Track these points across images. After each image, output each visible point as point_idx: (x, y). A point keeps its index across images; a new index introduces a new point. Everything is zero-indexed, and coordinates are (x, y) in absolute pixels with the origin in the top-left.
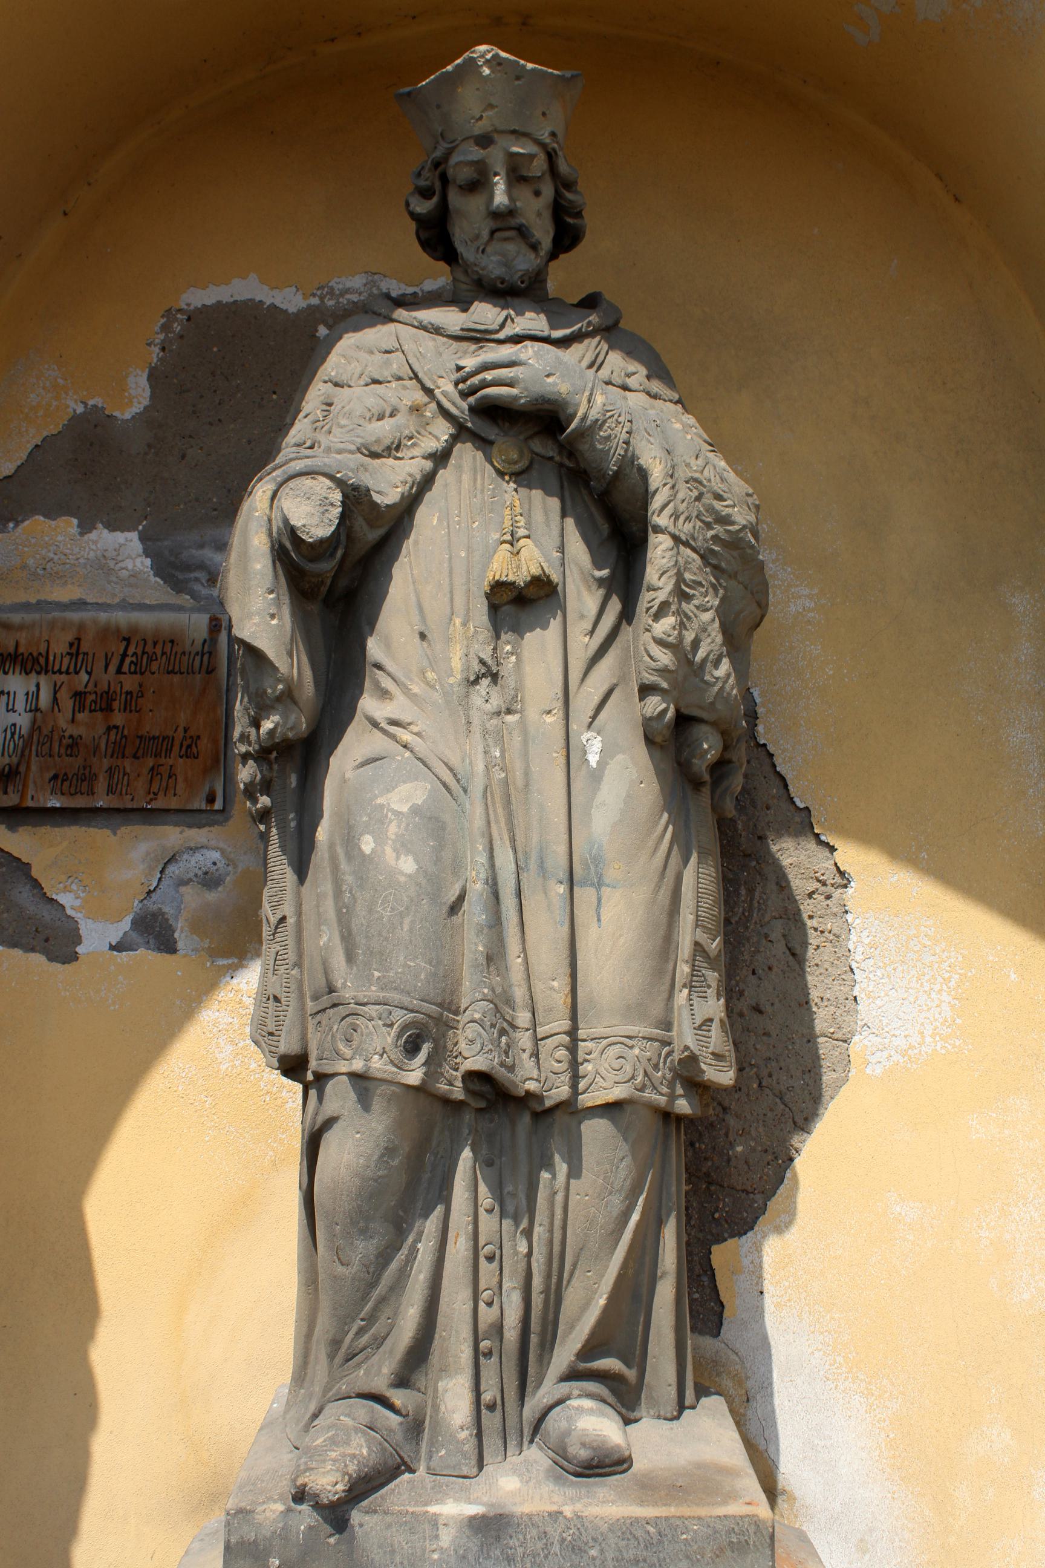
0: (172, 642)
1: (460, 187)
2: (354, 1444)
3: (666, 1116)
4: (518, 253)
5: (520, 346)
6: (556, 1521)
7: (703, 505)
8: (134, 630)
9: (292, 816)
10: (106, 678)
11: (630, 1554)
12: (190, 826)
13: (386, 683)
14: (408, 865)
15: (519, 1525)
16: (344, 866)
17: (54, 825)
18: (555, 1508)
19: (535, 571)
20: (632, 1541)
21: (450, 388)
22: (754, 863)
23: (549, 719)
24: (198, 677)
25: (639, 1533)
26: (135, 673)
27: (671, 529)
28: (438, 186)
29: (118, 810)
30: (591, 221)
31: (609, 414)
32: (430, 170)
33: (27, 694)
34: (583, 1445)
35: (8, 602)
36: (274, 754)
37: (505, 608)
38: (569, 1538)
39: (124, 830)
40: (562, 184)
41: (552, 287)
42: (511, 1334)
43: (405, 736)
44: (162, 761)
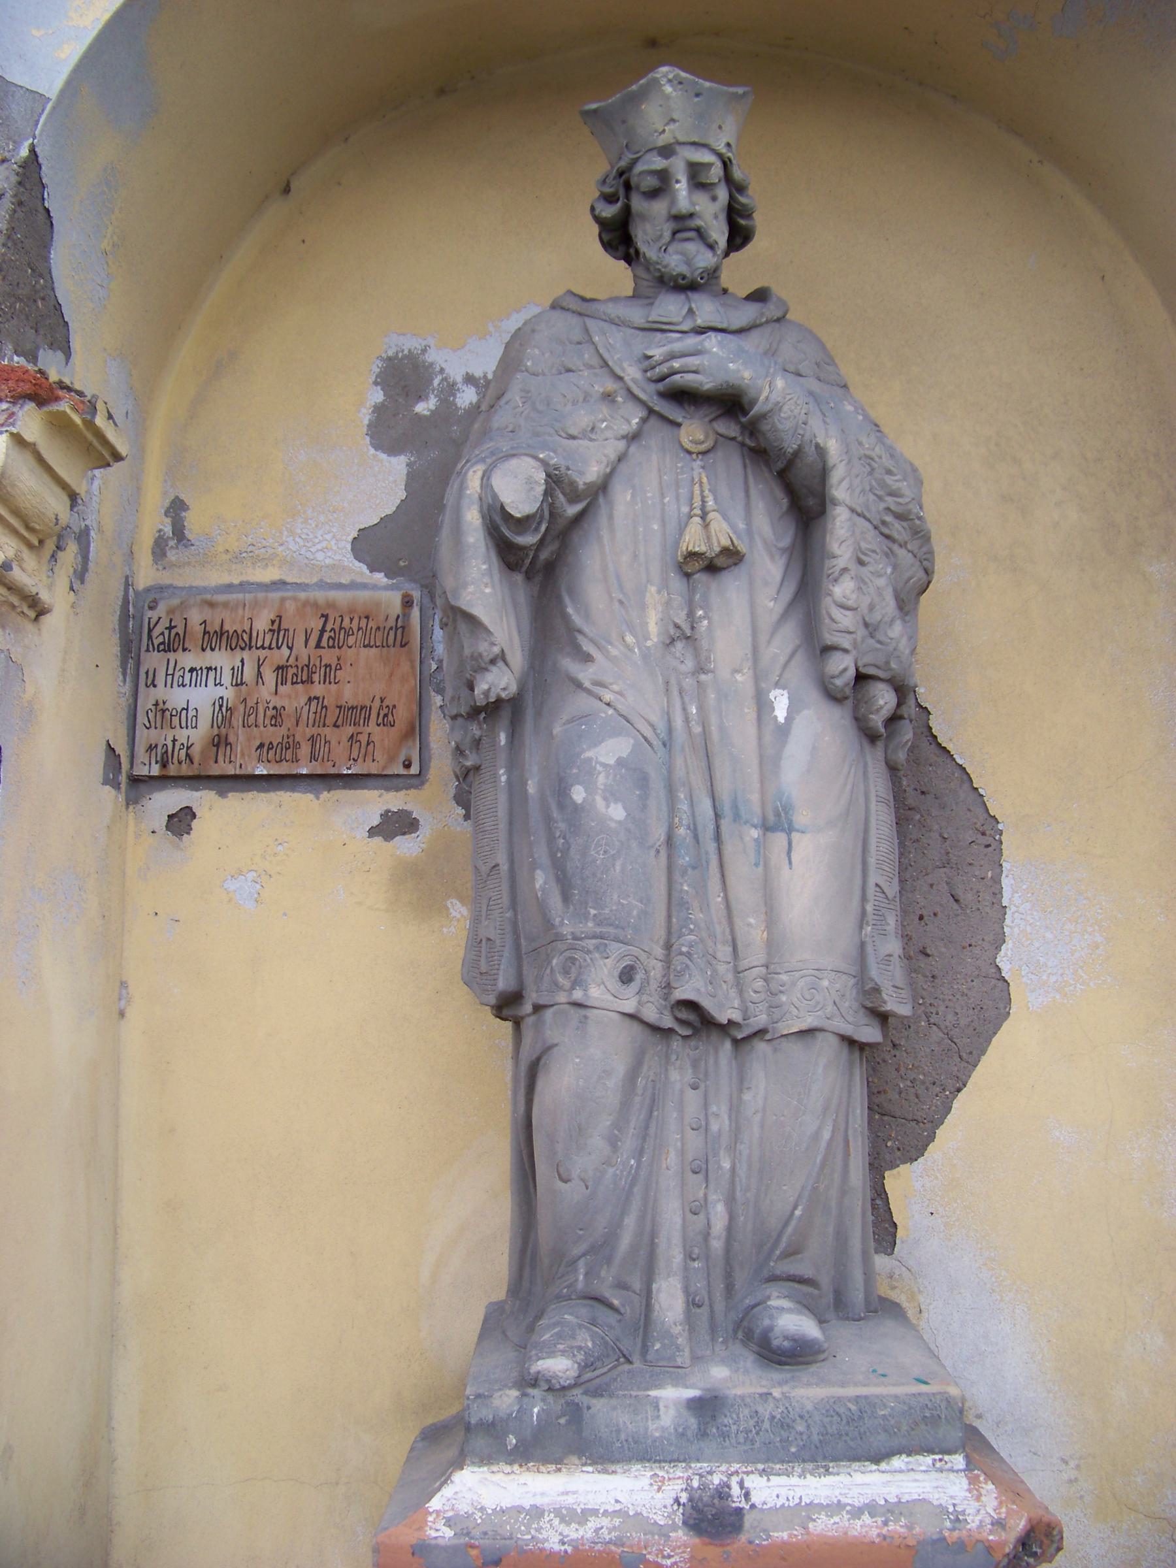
0: (367, 617)
1: (644, 193)
2: (579, 1338)
3: (850, 1042)
4: (698, 252)
5: (703, 336)
6: (766, 1401)
7: (876, 480)
8: (332, 605)
9: (502, 771)
10: (303, 652)
11: (833, 1429)
12: (388, 789)
13: (587, 647)
14: (617, 812)
15: (733, 1406)
16: (555, 814)
17: (259, 791)
18: (765, 1390)
19: (725, 542)
20: (836, 1418)
21: (638, 375)
22: (918, 817)
23: (739, 677)
24: (392, 650)
25: (842, 1410)
26: (333, 647)
27: (848, 502)
28: (622, 192)
30: (759, 220)
31: (788, 397)
32: (614, 178)
33: (233, 669)
34: (786, 1338)
35: (213, 584)
36: (483, 715)
37: (697, 576)
38: (778, 1416)
39: (325, 795)
40: (735, 187)
41: (725, 279)
42: (717, 1245)
43: (608, 697)
44: (361, 729)
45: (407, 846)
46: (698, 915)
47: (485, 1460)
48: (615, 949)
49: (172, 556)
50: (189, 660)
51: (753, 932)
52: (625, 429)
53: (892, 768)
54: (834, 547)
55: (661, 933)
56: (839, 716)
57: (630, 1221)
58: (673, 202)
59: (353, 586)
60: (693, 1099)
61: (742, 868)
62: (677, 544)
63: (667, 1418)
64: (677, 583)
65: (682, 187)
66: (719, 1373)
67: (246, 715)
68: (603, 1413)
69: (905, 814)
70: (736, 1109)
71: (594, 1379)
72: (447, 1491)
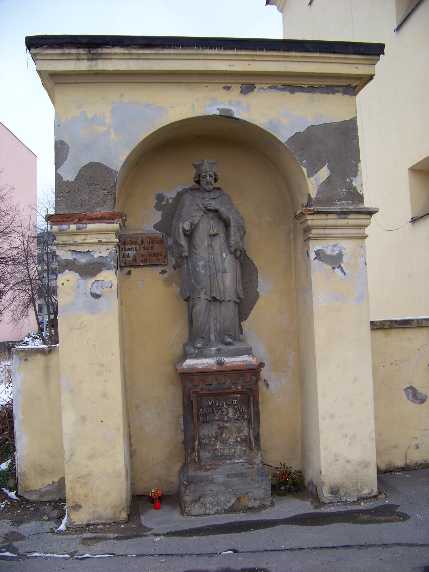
3: (235, 302)
8: (151, 237)
14: (203, 272)
29: (145, 265)
39: (152, 268)
42: (218, 330)
43: (201, 255)
45: (166, 275)
46: (214, 285)
47: (190, 358)
48: (205, 290)
49: (123, 229)
50: (128, 247)
51: (221, 286)
52: (201, 215)
53: (240, 262)
54: (232, 232)
55: (209, 287)
56: (232, 256)
57: (207, 327)
58: (207, 179)
59: (154, 233)
60: (214, 310)
61: (220, 278)
62: (209, 232)
63: (213, 352)
64: (209, 238)
65: (208, 177)
66: (220, 346)
67: (138, 255)
68: (205, 351)
69: (242, 268)
70: (220, 311)
71: (204, 347)
72: (185, 363)
